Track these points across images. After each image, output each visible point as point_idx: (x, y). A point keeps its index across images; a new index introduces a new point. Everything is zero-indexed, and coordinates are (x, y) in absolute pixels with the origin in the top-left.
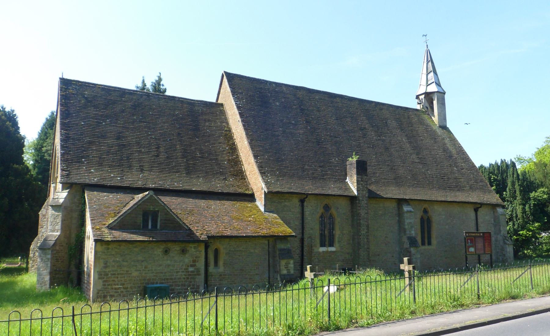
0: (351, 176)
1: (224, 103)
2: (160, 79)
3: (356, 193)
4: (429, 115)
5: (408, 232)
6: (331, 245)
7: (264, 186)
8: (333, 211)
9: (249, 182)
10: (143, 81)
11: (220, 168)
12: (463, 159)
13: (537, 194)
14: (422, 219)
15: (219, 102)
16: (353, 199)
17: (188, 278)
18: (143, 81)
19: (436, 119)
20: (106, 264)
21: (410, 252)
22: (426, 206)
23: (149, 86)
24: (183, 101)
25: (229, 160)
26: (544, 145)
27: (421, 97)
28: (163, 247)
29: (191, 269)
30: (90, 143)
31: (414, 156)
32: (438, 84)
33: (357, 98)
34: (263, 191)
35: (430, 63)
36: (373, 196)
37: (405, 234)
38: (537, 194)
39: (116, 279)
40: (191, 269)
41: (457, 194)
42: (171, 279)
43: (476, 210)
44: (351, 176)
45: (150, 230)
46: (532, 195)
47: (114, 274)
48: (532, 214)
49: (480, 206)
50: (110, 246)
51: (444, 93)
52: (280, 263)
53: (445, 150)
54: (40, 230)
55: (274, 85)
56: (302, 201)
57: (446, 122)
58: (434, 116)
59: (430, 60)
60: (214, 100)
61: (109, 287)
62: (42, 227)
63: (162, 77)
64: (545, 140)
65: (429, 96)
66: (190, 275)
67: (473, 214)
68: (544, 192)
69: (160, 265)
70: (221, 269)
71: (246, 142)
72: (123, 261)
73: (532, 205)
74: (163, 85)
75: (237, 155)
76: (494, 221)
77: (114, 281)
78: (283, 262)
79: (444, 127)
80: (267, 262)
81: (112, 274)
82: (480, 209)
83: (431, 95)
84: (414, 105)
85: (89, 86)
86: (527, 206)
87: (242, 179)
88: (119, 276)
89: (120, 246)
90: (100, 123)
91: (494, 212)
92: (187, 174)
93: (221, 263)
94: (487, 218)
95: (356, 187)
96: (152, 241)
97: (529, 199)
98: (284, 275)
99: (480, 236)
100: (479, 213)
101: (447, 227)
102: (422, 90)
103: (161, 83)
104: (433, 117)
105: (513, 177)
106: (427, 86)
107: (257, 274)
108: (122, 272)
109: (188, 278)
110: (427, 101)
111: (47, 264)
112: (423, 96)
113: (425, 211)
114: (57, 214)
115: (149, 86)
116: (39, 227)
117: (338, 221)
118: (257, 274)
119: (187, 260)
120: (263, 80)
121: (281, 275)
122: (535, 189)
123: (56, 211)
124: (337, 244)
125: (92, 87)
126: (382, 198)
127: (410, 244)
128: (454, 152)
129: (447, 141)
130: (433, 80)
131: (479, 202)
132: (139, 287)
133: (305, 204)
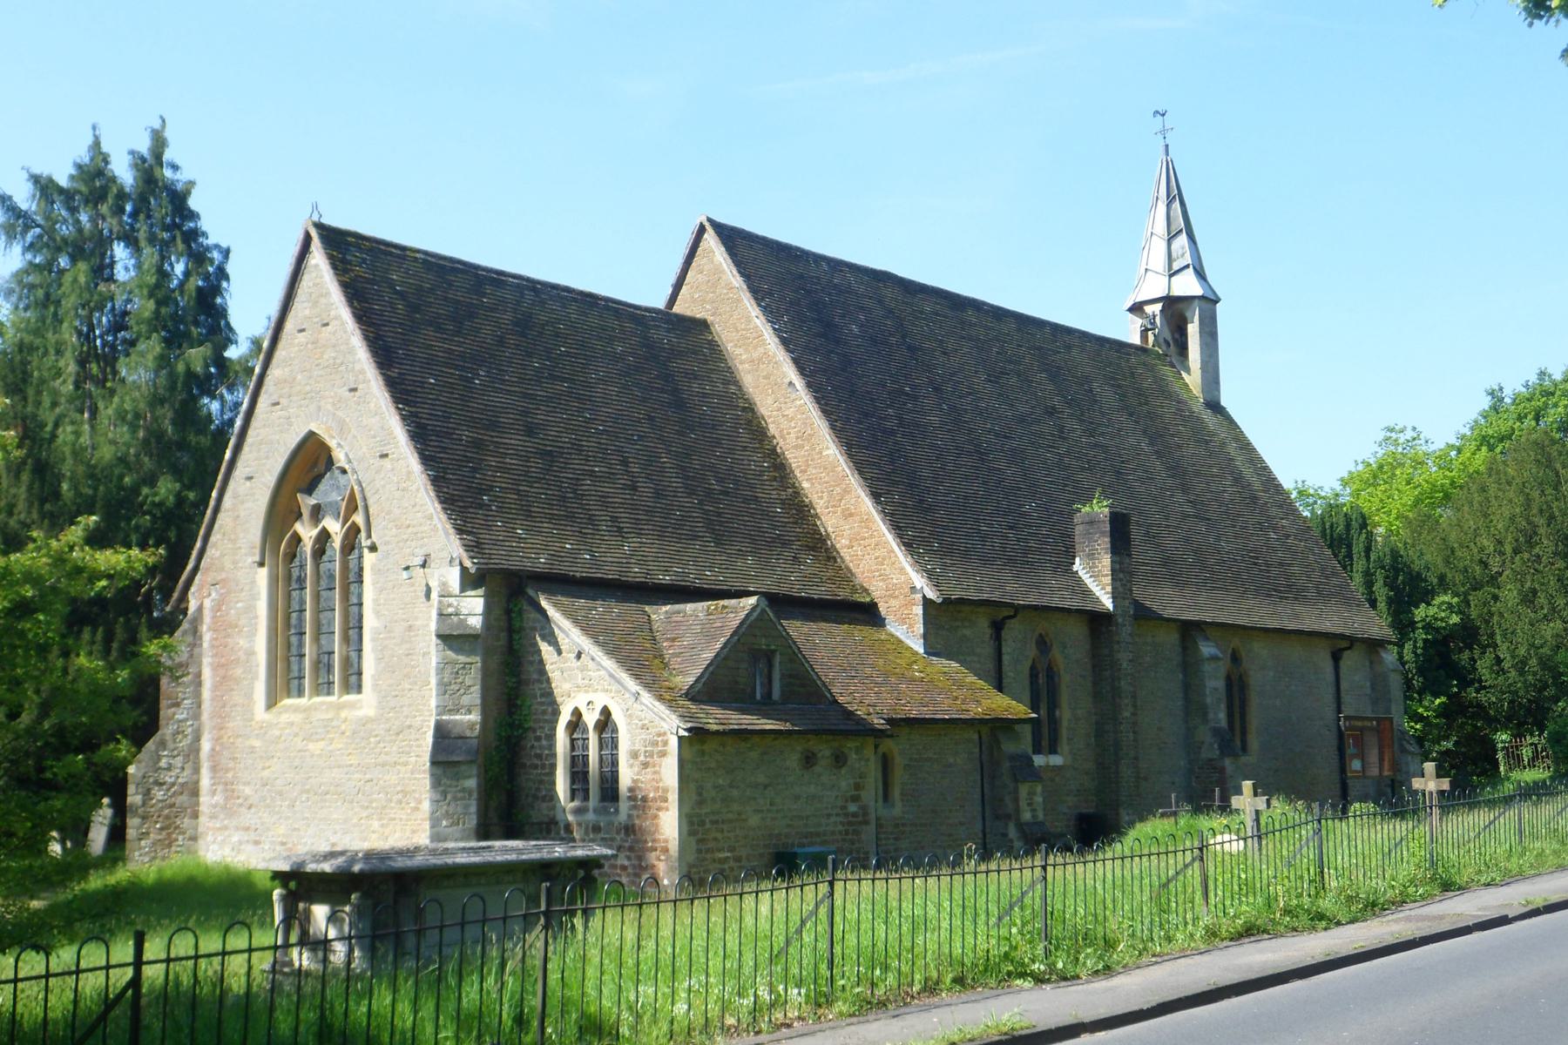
0: (1091, 556)
1: (710, 319)
2: (159, 141)
3: (1108, 603)
4: (1173, 366)
5: (1211, 716)
6: (1053, 750)
7: (919, 581)
8: (1056, 653)
9: (848, 568)
10: (97, 144)
11: (775, 527)
12: (1281, 506)
13: (1432, 611)
14: (1229, 678)
15: (676, 309)
16: (1097, 621)
17: (847, 833)
18: (97, 144)
19: (1193, 379)
20: (700, 794)
21: (1222, 770)
22: (1236, 642)
23: (123, 172)
24: (617, 310)
25: (783, 502)
26: (1381, 452)
27: (1149, 309)
28: (799, 748)
29: (853, 808)
30: (478, 444)
31: (1179, 497)
32: (1201, 274)
33: (896, 276)
34: (919, 596)
35: (1177, 205)
36: (1143, 615)
37: (1205, 720)
38: (1432, 611)
39: (719, 836)
40: (853, 808)
41: (1299, 608)
42: (818, 834)
43: (1336, 657)
44: (1091, 556)
45: (758, 703)
46: (1420, 613)
47: (716, 822)
48: (1421, 671)
49: (1344, 644)
50: (706, 747)
51: (1216, 301)
52: (1016, 790)
53: (1238, 479)
54: (164, 713)
55: (1047, 330)
56: (998, 627)
57: (1218, 390)
58: (1188, 371)
59: (1175, 195)
60: (655, 299)
61: (709, 856)
62: (177, 705)
63: (168, 134)
64: (1381, 435)
65: (1175, 308)
66: (850, 823)
67: (1328, 665)
68: (1450, 606)
69: (797, 798)
70: (898, 810)
71: (832, 451)
72: (731, 786)
73: (1420, 644)
74: (175, 168)
75: (793, 486)
76: (1373, 688)
77: (715, 839)
78: (1024, 790)
79: (1215, 406)
80: (978, 790)
81: (713, 822)
82: (1346, 654)
83: (1181, 306)
84: (1129, 331)
85: (391, 254)
86: (1408, 646)
87: (829, 558)
88: (725, 827)
89: (724, 745)
90: (467, 380)
91: (1371, 663)
92: (717, 544)
93: (896, 792)
94: (1356, 678)
95: (1109, 589)
96: (789, 732)
97: (1412, 624)
98: (1027, 824)
99: (1371, 729)
100: (1342, 663)
101: (1278, 702)
102: (1156, 287)
103: (168, 156)
104: (1184, 375)
105: (1368, 557)
106: (1171, 276)
107: (961, 824)
108: (730, 816)
109: (847, 833)
110: (1169, 323)
111: (466, 807)
112: (1157, 307)
113: (1235, 658)
114: (462, 659)
115: (123, 172)
116: (163, 703)
117: (1065, 679)
118: (961, 824)
119: (843, 784)
120: (798, 249)
121: (1021, 826)
122: (1426, 596)
123: (458, 651)
124: (1064, 747)
125: (398, 256)
126: (1160, 618)
127: (1220, 747)
128: (1257, 485)
129: (1232, 448)
130: (1188, 260)
131: (1347, 632)
132: (761, 855)
133: (1004, 633)
